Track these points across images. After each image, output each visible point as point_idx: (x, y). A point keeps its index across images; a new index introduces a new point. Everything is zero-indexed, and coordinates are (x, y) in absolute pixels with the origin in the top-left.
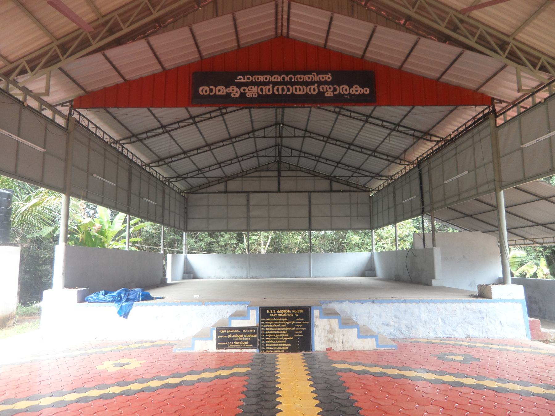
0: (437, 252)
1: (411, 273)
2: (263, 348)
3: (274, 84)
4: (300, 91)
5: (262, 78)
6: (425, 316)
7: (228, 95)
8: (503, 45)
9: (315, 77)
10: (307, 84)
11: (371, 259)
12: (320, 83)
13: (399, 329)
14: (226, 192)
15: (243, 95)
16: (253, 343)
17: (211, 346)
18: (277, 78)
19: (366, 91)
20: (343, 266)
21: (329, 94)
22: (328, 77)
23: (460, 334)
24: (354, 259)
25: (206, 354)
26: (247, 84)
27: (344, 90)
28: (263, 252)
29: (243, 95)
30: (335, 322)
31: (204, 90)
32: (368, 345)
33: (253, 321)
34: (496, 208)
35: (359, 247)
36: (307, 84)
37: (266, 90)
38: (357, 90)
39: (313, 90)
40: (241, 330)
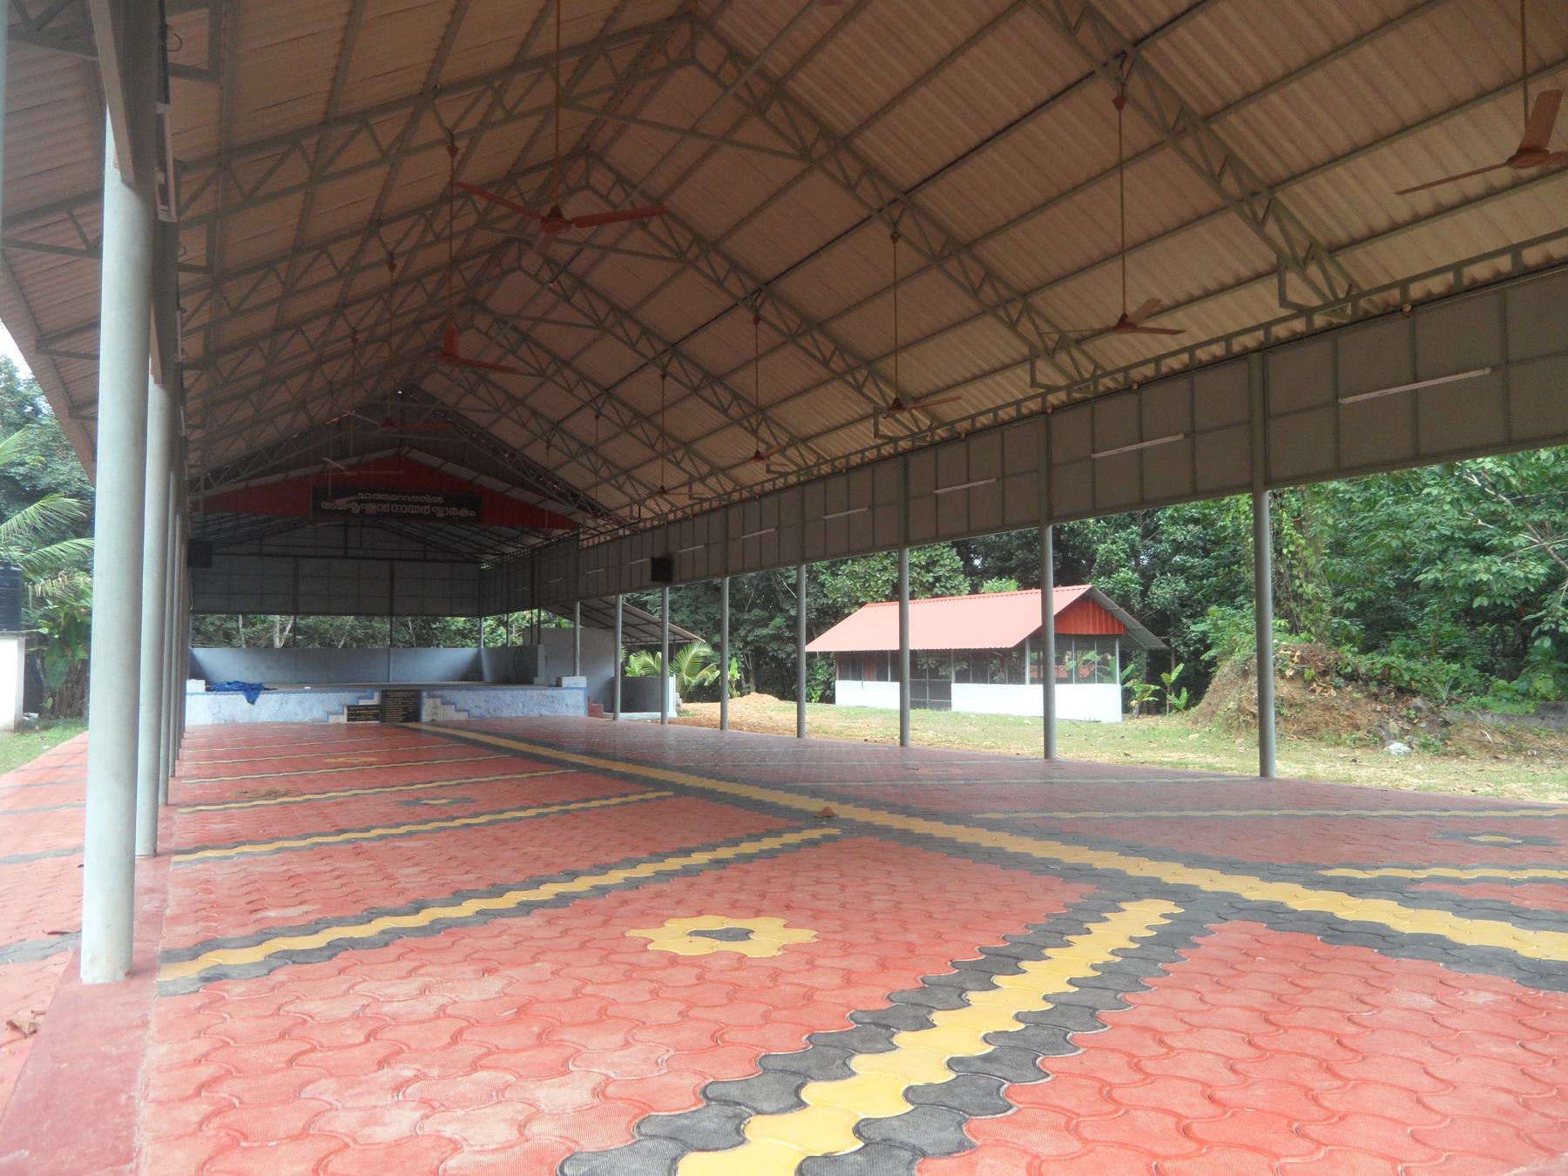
0: (541, 650)
1: (517, 669)
2: (383, 721)
3: (392, 503)
4: (414, 510)
5: (380, 496)
6: (509, 700)
7: (349, 510)
8: (575, 496)
9: (428, 499)
10: (422, 504)
11: (477, 657)
12: (433, 505)
13: (488, 710)
14: (259, 555)
15: (363, 511)
16: (376, 717)
17: (343, 719)
18: (395, 498)
19: (472, 514)
20: (446, 659)
21: (440, 515)
22: (440, 499)
23: (535, 713)
24: (455, 657)
25: (338, 725)
26: (367, 501)
27: (454, 511)
28: (278, 643)
29: (363, 511)
30: (438, 701)
31: (325, 505)
32: (463, 716)
33: (375, 700)
34: (614, 606)
35: (463, 634)
36: (422, 504)
37: (384, 508)
38: (464, 512)
39: (426, 510)
40: (366, 707)
